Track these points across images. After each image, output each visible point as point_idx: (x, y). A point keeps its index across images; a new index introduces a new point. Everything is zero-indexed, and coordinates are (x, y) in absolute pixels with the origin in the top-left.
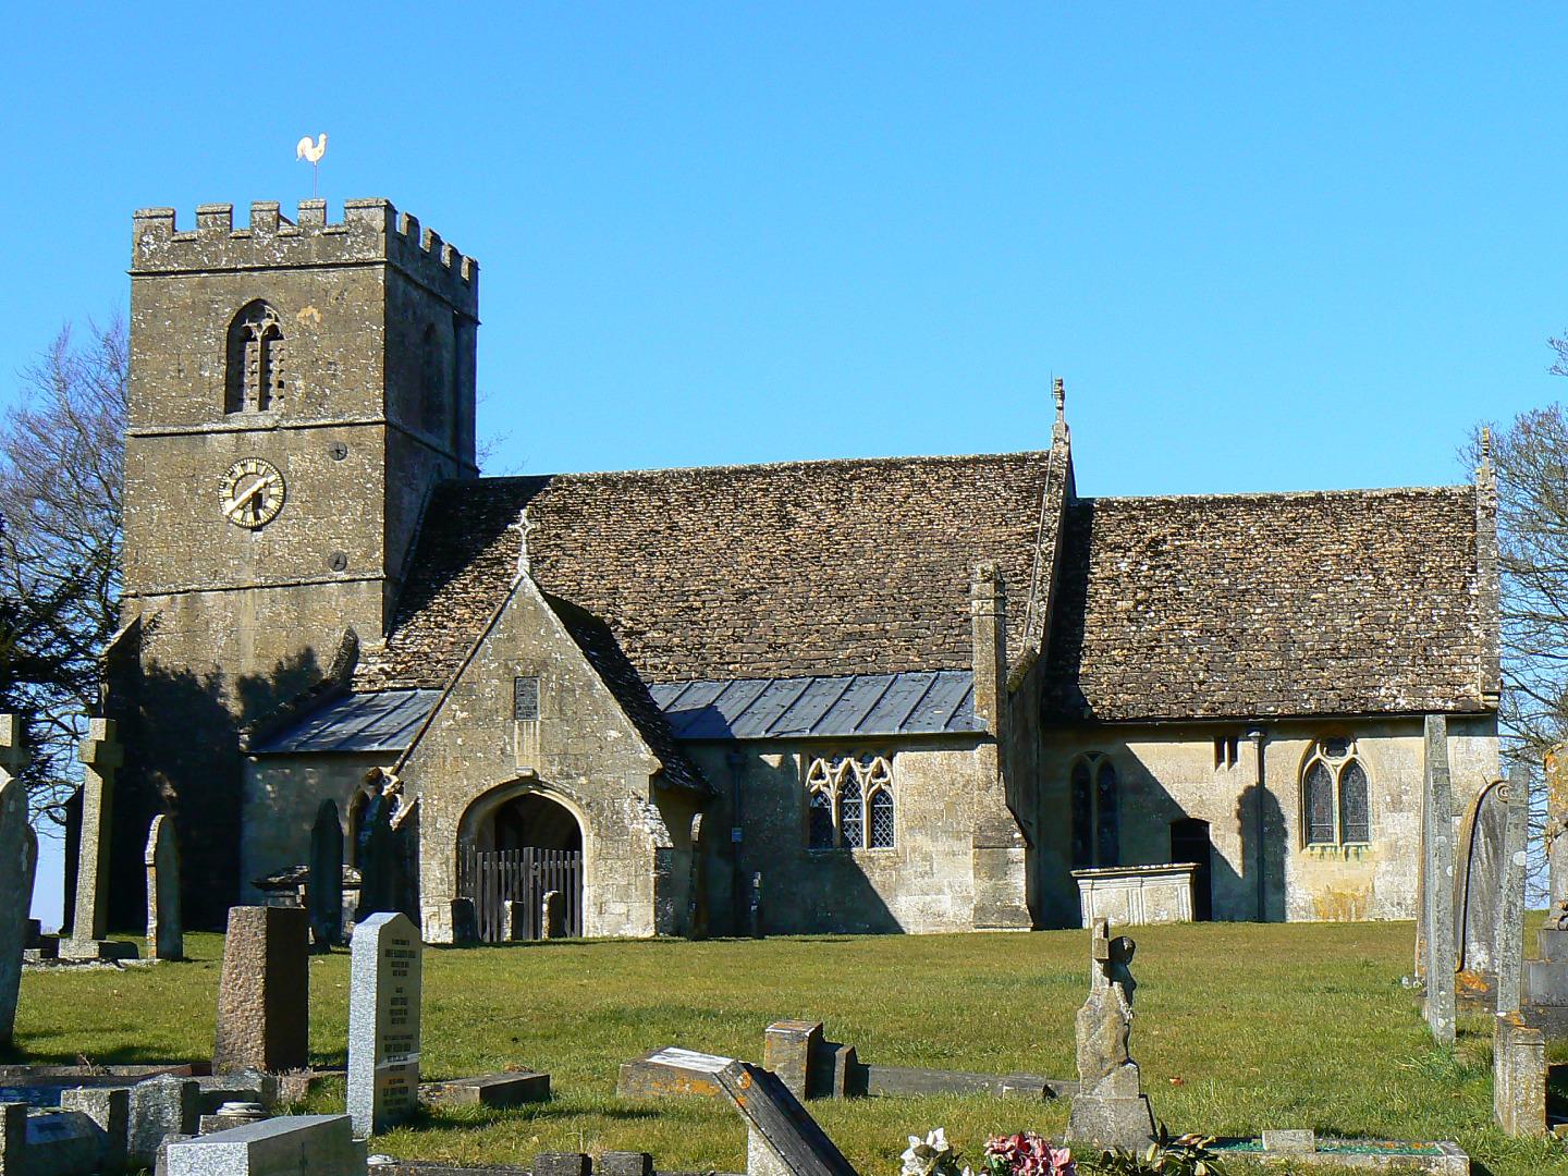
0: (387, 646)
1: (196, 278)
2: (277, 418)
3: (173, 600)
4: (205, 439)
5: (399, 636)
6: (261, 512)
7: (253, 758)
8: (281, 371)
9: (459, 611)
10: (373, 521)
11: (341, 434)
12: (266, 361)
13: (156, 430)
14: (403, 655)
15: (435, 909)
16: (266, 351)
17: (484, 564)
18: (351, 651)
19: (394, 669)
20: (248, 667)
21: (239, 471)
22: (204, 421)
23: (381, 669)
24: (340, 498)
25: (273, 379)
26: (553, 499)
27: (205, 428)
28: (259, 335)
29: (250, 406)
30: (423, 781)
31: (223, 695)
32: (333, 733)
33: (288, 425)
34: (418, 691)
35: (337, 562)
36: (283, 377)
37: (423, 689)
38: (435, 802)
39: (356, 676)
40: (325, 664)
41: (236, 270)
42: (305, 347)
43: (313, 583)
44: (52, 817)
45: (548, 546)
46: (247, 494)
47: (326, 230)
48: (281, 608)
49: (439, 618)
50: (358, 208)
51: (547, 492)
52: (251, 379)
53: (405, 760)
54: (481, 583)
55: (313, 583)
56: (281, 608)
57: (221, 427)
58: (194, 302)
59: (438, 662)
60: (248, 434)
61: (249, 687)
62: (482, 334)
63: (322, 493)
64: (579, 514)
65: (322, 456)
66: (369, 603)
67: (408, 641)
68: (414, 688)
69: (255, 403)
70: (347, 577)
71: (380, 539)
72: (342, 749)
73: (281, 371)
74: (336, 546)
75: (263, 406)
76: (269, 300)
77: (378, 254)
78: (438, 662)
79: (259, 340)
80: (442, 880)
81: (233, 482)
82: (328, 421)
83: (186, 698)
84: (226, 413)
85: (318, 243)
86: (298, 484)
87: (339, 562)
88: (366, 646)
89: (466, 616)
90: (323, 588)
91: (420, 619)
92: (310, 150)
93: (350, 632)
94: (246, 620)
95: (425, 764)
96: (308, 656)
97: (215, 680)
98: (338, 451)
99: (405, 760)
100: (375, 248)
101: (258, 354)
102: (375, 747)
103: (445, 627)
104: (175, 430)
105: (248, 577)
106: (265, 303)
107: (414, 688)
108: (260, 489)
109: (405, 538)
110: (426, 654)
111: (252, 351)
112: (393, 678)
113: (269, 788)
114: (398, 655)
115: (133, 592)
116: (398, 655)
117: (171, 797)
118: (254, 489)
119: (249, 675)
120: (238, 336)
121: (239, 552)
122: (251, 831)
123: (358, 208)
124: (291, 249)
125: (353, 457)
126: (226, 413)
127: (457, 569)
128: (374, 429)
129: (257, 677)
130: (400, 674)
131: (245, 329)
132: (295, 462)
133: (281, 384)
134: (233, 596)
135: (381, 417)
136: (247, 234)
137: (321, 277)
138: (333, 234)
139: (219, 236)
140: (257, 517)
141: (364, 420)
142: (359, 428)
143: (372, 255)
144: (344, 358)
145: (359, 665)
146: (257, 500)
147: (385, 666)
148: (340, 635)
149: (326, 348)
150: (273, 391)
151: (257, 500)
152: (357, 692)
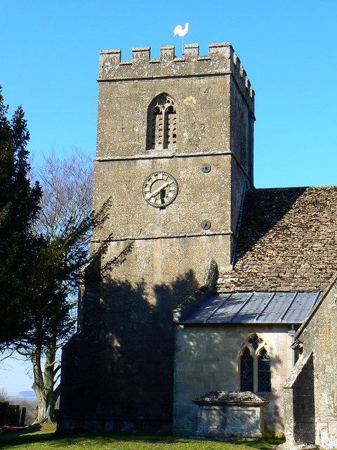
0: (233, 269)
1: (131, 83)
2: (174, 152)
3: (118, 244)
4: (135, 163)
5: (239, 264)
6: (165, 199)
7: (182, 326)
8: (175, 129)
9: (270, 252)
10: (225, 204)
11: (208, 160)
12: (167, 124)
13: (110, 158)
14: (243, 274)
15: (326, 424)
16: (167, 119)
17: (278, 229)
18: (215, 272)
19: (239, 281)
20: (159, 279)
21: (154, 179)
22: (135, 153)
23: (232, 281)
24: (207, 192)
25: (170, 133)
26: (309, 198)
27: (136, 157)
28: (163, 111)
29: (159, 147)
30: (316, 342)
31: (147, 294)
32: (223, 314)
33: (180, 155)
34: (254, 292)
35: (206, 225)
36: (176, 132)
37: (256, 291)
38: (324, 356)
39: (219, 284)
40: (202, 280)
41: (152, 79)
42: (188, 117)
43: (193, 236)
44: (20, 353)
45: (312, 220)
46: (158, 190)
47: (199, 58)
48: (175, 249)
49: (259, 256)
50: (216, 47)
51: (306, 195)
52: (159, 134)
53: (303, 328)
54: (279, 238)
55: (193, 236)
56: (175, 249)
57: (144, 156)
58: (130, 95)
59: (263, 278)
60: (158, 160)
61: (160, 290)
62: (256, 124)
63: (198, 189)
64: (325, 205)
65: (198, 171)
66: (222, 248)
67: (244, 267)
68: (252, 291)
69: (162, 145)
70: (212, 233)
71: (229, 213)
72: (234, 321)
73: (175, 129)
74: (205, 217)
75: (165, 147)
76: (169, 93)
77: (228, 70)
78: (263, 278)
79: (163, 113)
80: (330, 406)
81: (150, 184)
82: (201, 153)
83: (128, 295)
84: (147, 149)
85: (195, 65)
86: (185, 185)
87: (207, 225)
88: (222, 269)
89: (274, 254)
90: (198, 238)
91: (249, 255)
92: (180, 31)
93: (213, 261)
94: (157, 255)
95: (317, 331)
96: (191, 274)
97: (141, 286)
98: (206, 168)
99: (303, 328)
100: (225, 66)
101: (163, 126)
102: (254, 321)
103: (263, 260)
104: (120, 158)
105: (158, 232)
106: (167, 95)
107: (252, 291)
108: (165, 187)
109: (237, 215)
110: (256, 273)
111: (160, 120)
112: (240, 286)
113: (191, 343)
114: (241, 274)
115: (97, 240)
116: (241, 274)
117: (117, 347)
118: (162, 187)
119: (159, 283)
120: (153, 112)
121: (154, 221)
122: (179, 368)
123: (216, 47)
124: (181, 68)
125: (214, 171)
126: (147, 149)
127: (265, 232)
128: (226, 157)
129: (164, 284)
130: (243, 283)
131: (157, 107)
132: (183, 174)
133: (174, 136)
134: (150, 242)
135: (229, 151)
136: (158, 61)
137: (197, 82)
138: (203, 60)
139: (144, 62)
140: (163, 202)
141: (220, 152)
142: (217, 156)
143: (224, 70)
144: (209, 122)
145: (219, 279)
146: (163, 193)
147: (234, 279)
148: (208, 264)
149: (199, 116)
150: (171, 139)
151: (163, 193)
152: (220, 293)
